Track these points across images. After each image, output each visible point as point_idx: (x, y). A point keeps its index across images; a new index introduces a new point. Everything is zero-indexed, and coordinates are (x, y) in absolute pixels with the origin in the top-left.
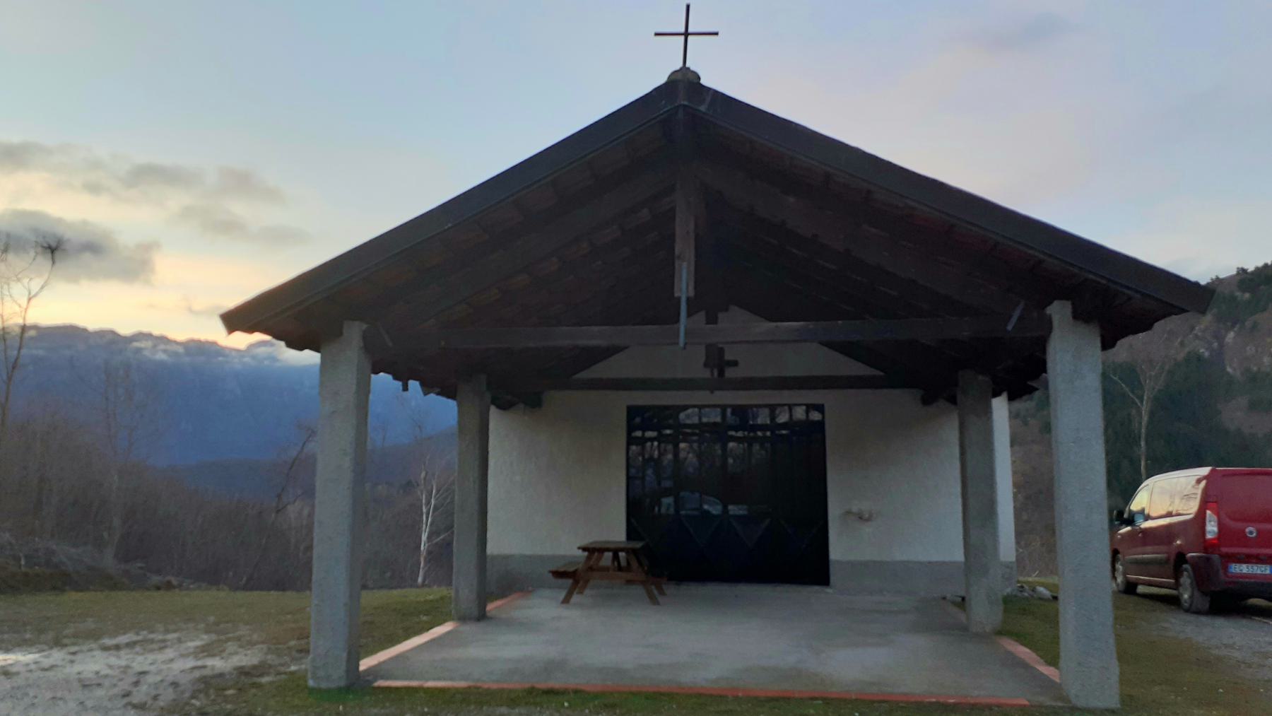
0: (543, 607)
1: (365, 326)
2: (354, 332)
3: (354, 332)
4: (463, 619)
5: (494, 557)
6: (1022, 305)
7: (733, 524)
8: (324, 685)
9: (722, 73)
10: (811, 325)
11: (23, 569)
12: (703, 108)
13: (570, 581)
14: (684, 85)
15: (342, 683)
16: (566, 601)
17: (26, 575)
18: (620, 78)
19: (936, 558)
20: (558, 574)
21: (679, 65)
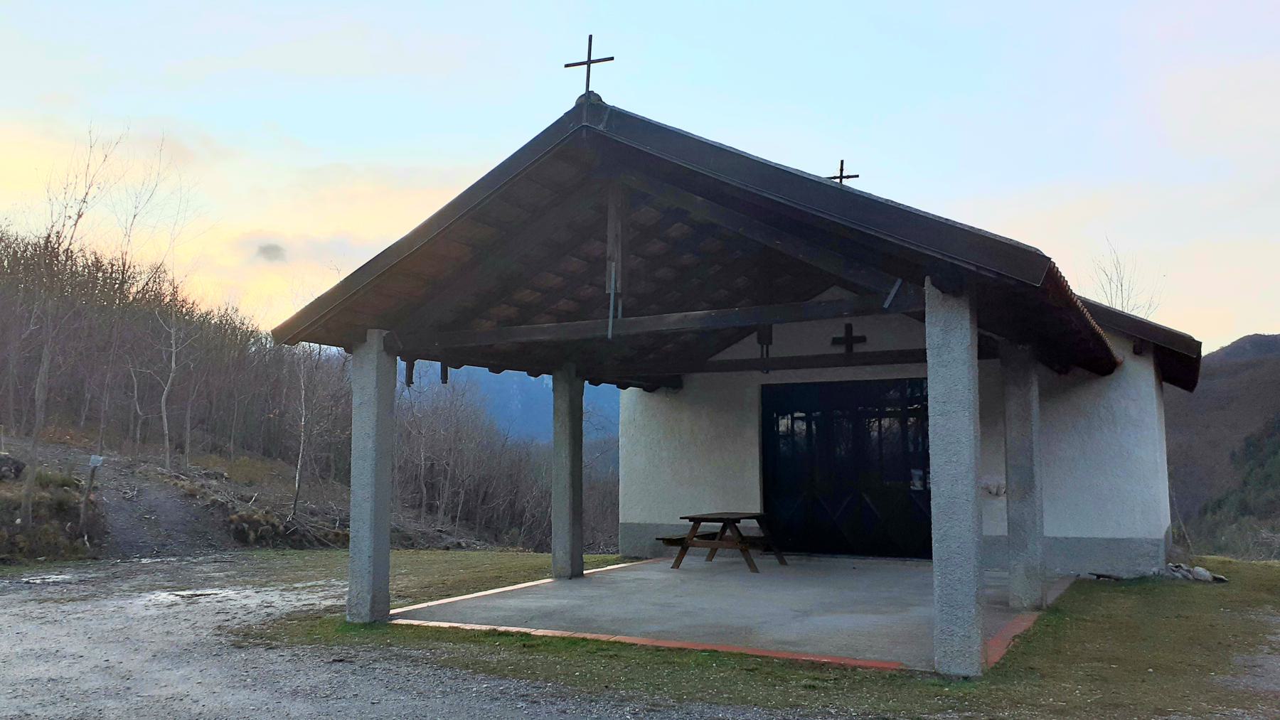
0: (656, 573)
1: (385, 333)
2: (375, 339)
3: (375, 339)
4: (558, 577)
5: (629, 526)
6: (899, 281)
7: (839, 496)
8: (357, 621)
9: (618, 92)
10: (713, 313)
11: (336, 530)
12: (601, 127)
13: (677, 549)
14: (590, 102)
15: (367, 620)
16: (677, 565)
17: (337, 535)
18: (556, 102)
19: (1072, 534)
20: (670, 542)
21: (584, 92)
